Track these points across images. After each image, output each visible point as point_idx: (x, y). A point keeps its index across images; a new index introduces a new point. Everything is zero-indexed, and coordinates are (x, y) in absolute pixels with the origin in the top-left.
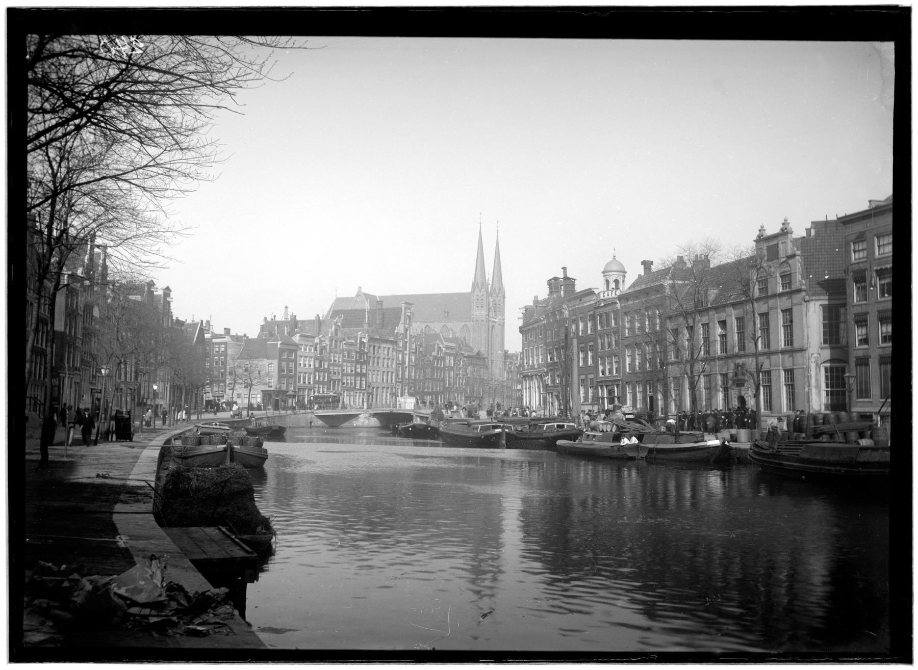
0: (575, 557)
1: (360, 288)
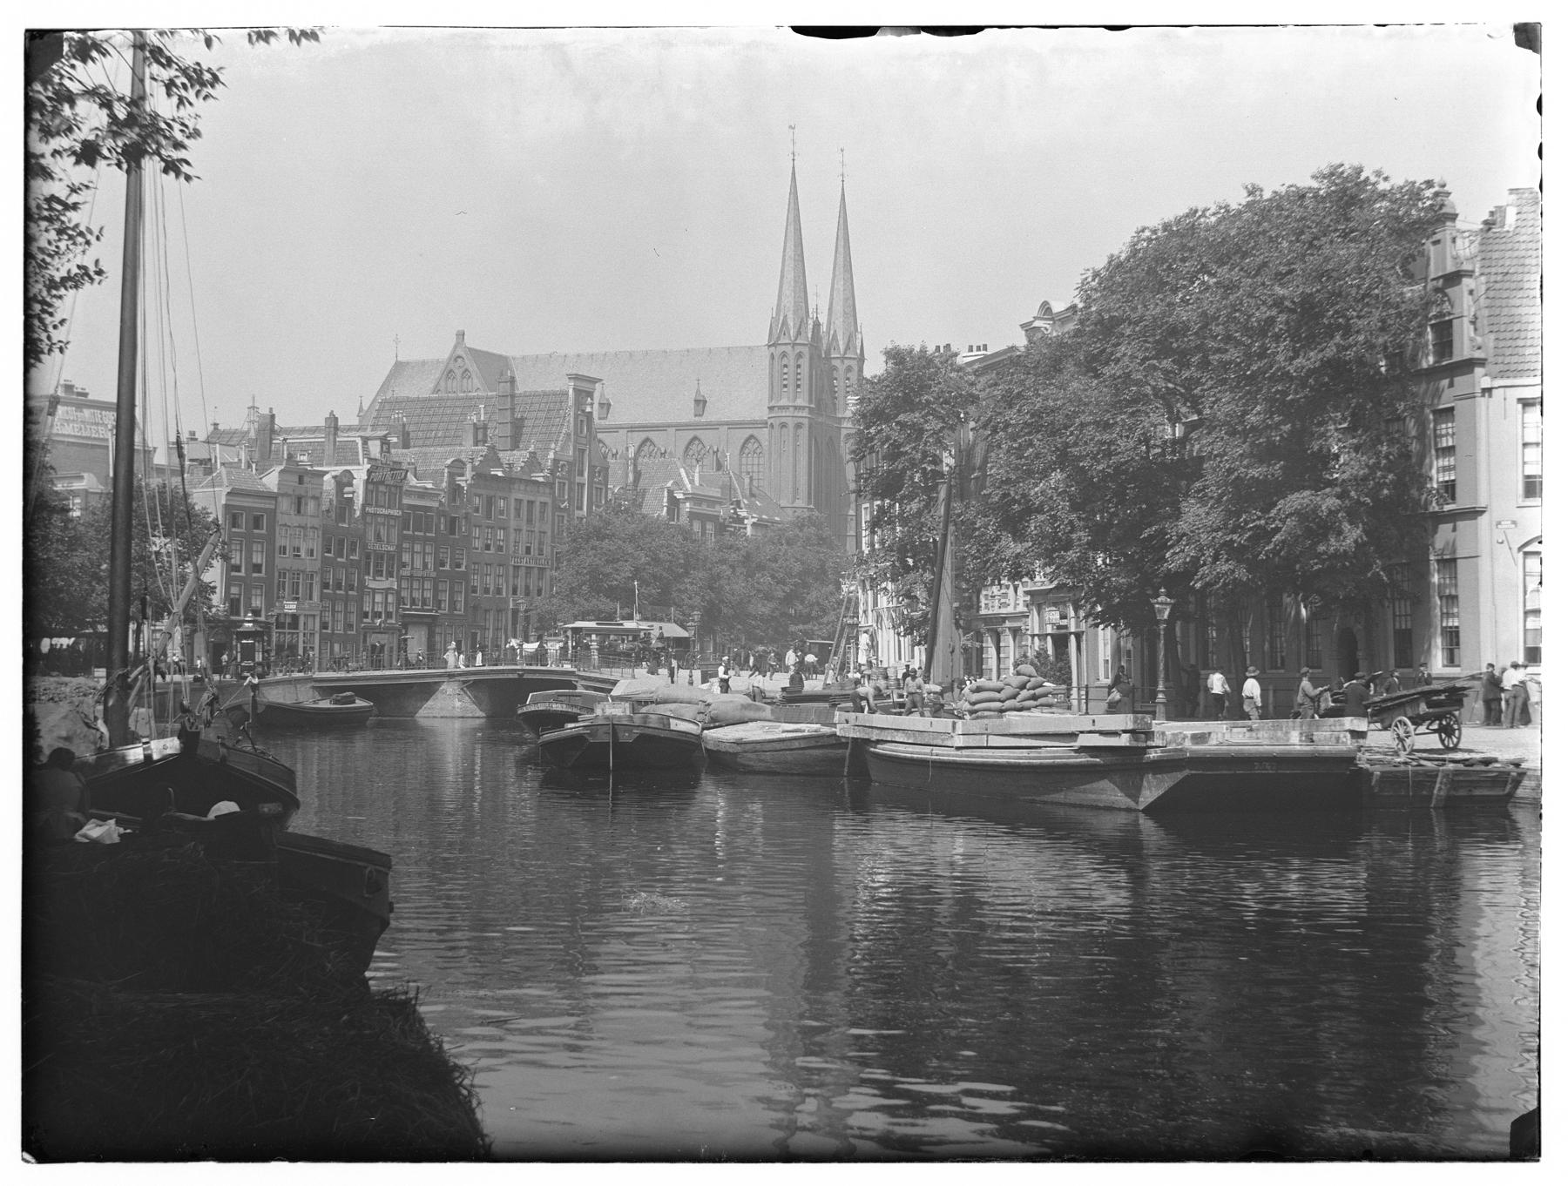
0: (367, 1032)
1: (461, 335)
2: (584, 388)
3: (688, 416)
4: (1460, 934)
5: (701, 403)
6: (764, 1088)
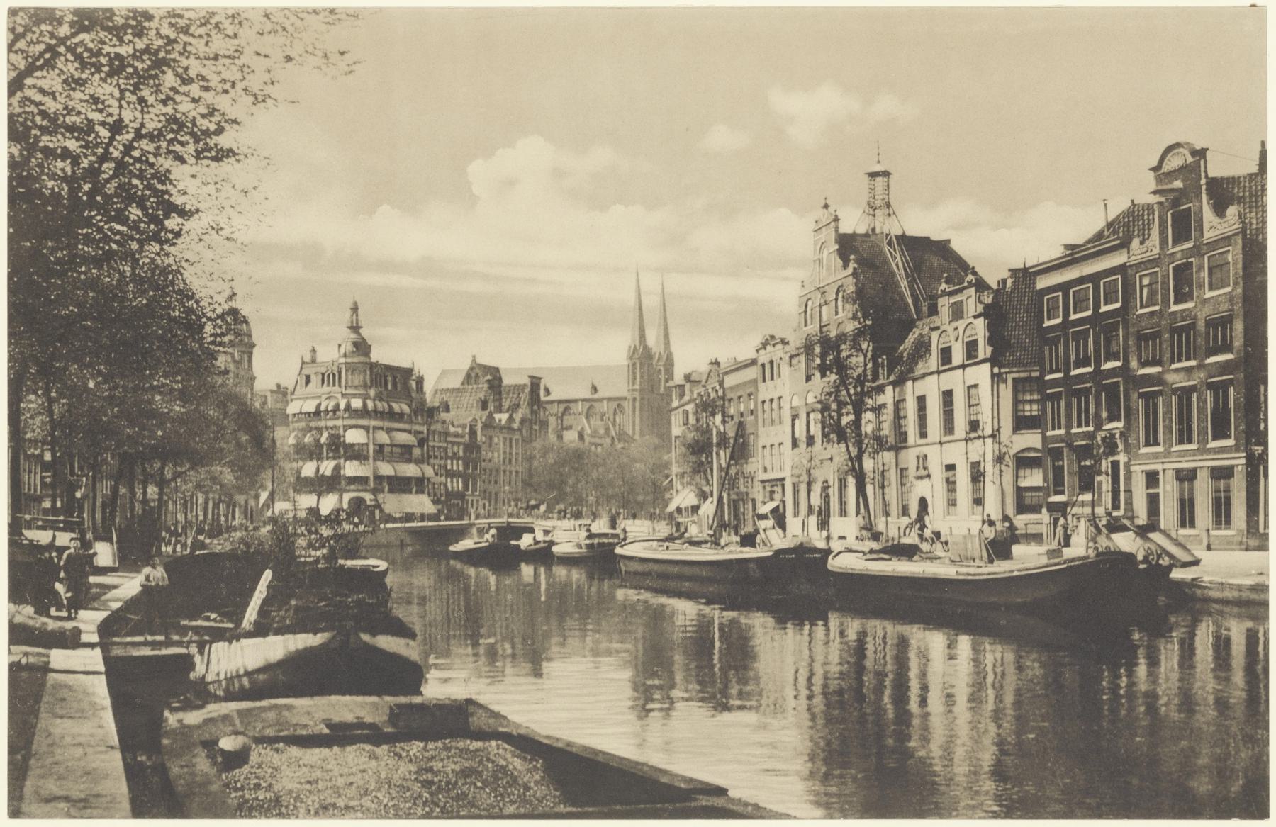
2: (535, 383)
3: (587, 394)
4: (435, 705)
5: (595, 389)
6: (807, 798)
